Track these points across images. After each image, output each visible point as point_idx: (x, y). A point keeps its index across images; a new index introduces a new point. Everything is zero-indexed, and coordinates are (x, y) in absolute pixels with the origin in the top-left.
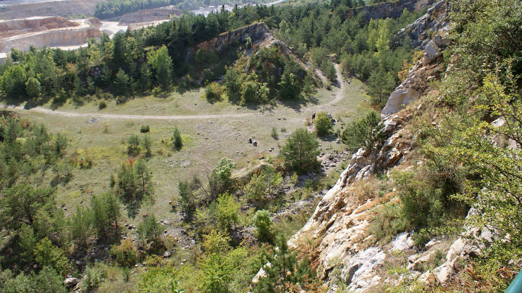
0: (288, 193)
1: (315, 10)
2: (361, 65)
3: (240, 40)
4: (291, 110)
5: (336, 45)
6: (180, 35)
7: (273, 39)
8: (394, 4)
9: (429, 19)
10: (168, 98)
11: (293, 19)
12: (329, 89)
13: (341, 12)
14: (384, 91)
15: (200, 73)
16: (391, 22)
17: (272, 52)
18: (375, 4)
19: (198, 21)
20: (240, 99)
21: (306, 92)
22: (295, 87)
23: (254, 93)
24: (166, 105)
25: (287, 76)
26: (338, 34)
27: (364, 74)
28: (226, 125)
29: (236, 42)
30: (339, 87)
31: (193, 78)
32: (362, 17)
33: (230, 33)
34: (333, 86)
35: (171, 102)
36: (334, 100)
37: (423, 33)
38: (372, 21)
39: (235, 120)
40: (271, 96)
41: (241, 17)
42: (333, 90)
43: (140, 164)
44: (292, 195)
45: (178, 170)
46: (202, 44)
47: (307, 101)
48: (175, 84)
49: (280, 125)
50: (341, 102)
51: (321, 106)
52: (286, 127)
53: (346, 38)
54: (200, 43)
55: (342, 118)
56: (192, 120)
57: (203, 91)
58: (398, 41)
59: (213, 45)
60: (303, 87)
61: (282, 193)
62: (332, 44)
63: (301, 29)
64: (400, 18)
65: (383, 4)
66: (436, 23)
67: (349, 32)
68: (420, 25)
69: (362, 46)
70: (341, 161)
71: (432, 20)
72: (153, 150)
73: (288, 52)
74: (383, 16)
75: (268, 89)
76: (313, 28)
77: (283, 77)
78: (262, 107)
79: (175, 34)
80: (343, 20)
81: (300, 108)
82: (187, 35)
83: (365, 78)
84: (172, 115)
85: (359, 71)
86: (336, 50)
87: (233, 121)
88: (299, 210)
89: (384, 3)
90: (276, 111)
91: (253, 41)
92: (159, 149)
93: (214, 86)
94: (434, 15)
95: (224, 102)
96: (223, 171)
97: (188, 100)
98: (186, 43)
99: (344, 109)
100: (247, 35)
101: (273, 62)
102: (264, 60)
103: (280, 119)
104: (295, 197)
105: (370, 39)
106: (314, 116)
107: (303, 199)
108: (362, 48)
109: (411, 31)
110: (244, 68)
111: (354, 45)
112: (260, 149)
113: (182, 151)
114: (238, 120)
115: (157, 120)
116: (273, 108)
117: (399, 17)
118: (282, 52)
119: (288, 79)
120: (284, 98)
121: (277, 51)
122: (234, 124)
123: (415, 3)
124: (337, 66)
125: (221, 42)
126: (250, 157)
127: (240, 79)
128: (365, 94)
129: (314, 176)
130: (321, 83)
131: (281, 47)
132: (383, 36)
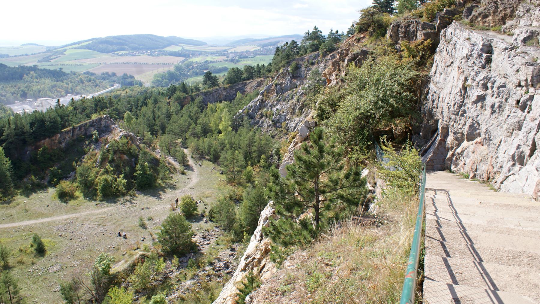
0: (173, 276)
1: (153, 98)
2: (210, 147)
3: (85, 134)
4: (152, 199)
5: (182, 131)
6: (16, 134)
7: (121, 131)
8: (227, 88)
9: (262, 100)
10: (13, 204)
11: (132, 108)
12: (183, 174)
13: (178, 99)
14: (237, 168)
15: (45, 173)
16: (227, 105)
17: (123, 144)
18: (209, 89)
19: (36, 118)
20: (96, 195)
21: (162, 179)
22: (151, 175)
23: (111, 186)
24: (12, 211)
25: (142, 166)
26: (180, 120)
27: (214, 155)
28: (89, 222)
29: (81, 137)
30: (192, 170)
31: (39, 178)
32: (200, 102)
33: (74, 128)
34: (186, 171)
35: (17, 208)
36: (191, 183)
37: (259, 113)
38: (210, 105)
39: (97, 217)
40: (129, 187)
41: (80, 110)
42: (187, 174)
43: (6, 277)
44: (178, 278)
45: (48, 276)
46: (42, 141)
47: (165, 187)
48: (17, 187)
49: (145, 215)
50: (198, 185)
51: (180, 191)
52: (152, 215)
53: (190, 124)
54: (40, 140)
55: (203, 199)
56: (49, 222)
57: (52, 191)
58: (238, 121)
59: (56, 141)
60: (158, 174)
61: (166, 278)
62: (177, 131)
63: (141, 119)
64: (235, 101)
65: (217, 89)
66: (269, 103)
67: (190, 117)
68: (255, 106)
69: (205, 129)
70: (214, 238)
71: (265, 101)
72: (11, 261)
73: (138, 142)
74: (218, 99)
75: (125, 181)
76: (155, 117)
77: (138, 166)
78: (122, 199)
79: (11, 133)
80: (182, 107)
81: (160, 195)
82: (25, 133)
83: (215, 159)
84: (23, 220)
85: (209, 153)
86: (182, 136)
87: (95, 217)
88: (188, 289)
89: (217, 87)
90: (136, 201)
91: (99, 134)
92: (18, 259)
93: (65, 185)
94: (266, 96)
95: (79, 199)
96: (104, 267)
97: (38, 203)
98: (25, 142)
99: (203, 190)
100: (92, 129)
101: (125, 154)
102: (115, 152)
103: (143, 209)
104: (180, 279)
105: (212, 122)
106: (177, 201)
107: (189, 278)
108: (206, 131)
109: (248, 112)
110: (95, 162)
111: (198, 129)
112: (132, 241)
113: (46, 256)
114: (100, 216)
115: (5, 229)
116: (133, 199)
117: (234, 99)
118: (133, 142)
119: (143, 167)
120: (142, 188)
121: (128, 142)
122: (97, 220)
123: (245, 86)
124: (186, 151)
125: (65, 139)
126: (124, 249)
127: (93, 175)
128: (218, 173)
129: (193, 256)
130: (175, 168)
131: (131, 138)
132: (225, 118)
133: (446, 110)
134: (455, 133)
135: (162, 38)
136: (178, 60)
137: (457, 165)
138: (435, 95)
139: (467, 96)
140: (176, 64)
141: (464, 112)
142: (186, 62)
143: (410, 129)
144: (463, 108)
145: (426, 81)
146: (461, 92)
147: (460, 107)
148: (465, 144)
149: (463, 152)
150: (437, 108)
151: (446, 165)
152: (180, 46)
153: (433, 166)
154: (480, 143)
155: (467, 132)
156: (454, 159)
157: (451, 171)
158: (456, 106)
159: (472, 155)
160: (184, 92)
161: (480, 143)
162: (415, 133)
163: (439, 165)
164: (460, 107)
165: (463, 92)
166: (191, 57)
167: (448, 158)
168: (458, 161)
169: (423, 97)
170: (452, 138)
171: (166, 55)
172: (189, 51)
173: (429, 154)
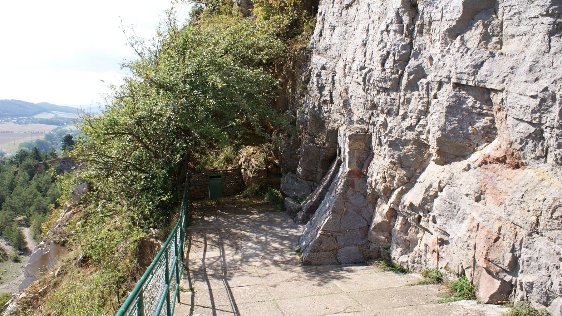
5: (24, 206)
12: (16, 260)
13: (28, 167)
42: (22, 261)
133: (357, 93)
134: (393, 145)
135: (32, 105)
136: (49, 129)
137: (408, 246)
138: (323, 72)
139: (422, 25)
140: (47, 132)
141: (420, 73)
142: (59, 130)
143: (275, 165)
144: (413, 63)
145: (304, 59)
146: (400, 22)
147: (404, 61)
148: (433, 173)
149: (428, 200)
150: (332, 102)
151: (373, 246)
152: (54, 113)
153: (335, 252)
154: (502, 161)
155: (443, 129)
156: (398, 226)
157: (391, 265)
158: (389, 63)
159: (475, 212)
160: (37, 159)
161: (502, 161)
162: (287, 170)
163: (352, 248)
164: (404, 61)
165: (406, 19)
166: (65, 126)
167: (379, 225)
168: (411, 232)
169: (299, 90)
170: (387, 162)
171: (35, 123)
172: (63, 118)
173: (321, 215)
